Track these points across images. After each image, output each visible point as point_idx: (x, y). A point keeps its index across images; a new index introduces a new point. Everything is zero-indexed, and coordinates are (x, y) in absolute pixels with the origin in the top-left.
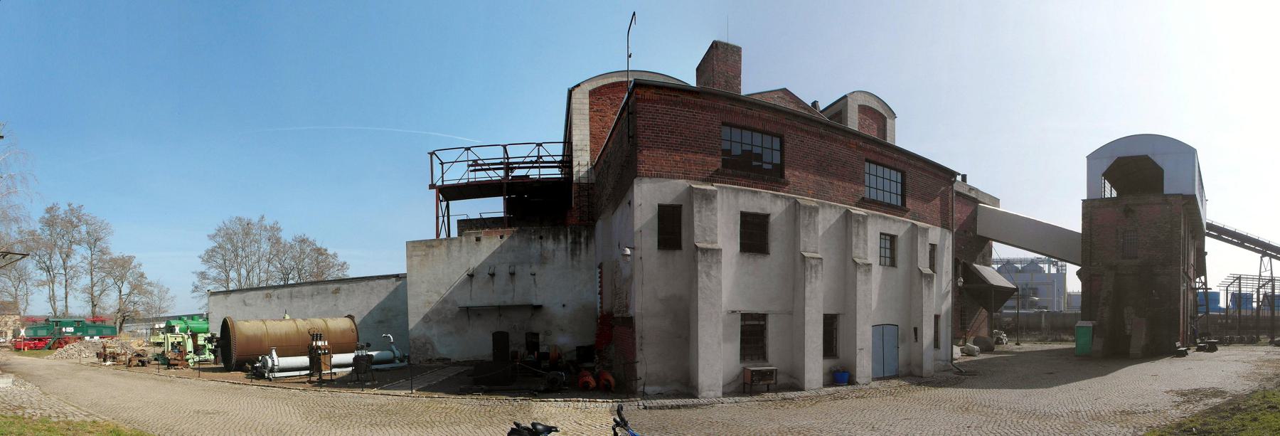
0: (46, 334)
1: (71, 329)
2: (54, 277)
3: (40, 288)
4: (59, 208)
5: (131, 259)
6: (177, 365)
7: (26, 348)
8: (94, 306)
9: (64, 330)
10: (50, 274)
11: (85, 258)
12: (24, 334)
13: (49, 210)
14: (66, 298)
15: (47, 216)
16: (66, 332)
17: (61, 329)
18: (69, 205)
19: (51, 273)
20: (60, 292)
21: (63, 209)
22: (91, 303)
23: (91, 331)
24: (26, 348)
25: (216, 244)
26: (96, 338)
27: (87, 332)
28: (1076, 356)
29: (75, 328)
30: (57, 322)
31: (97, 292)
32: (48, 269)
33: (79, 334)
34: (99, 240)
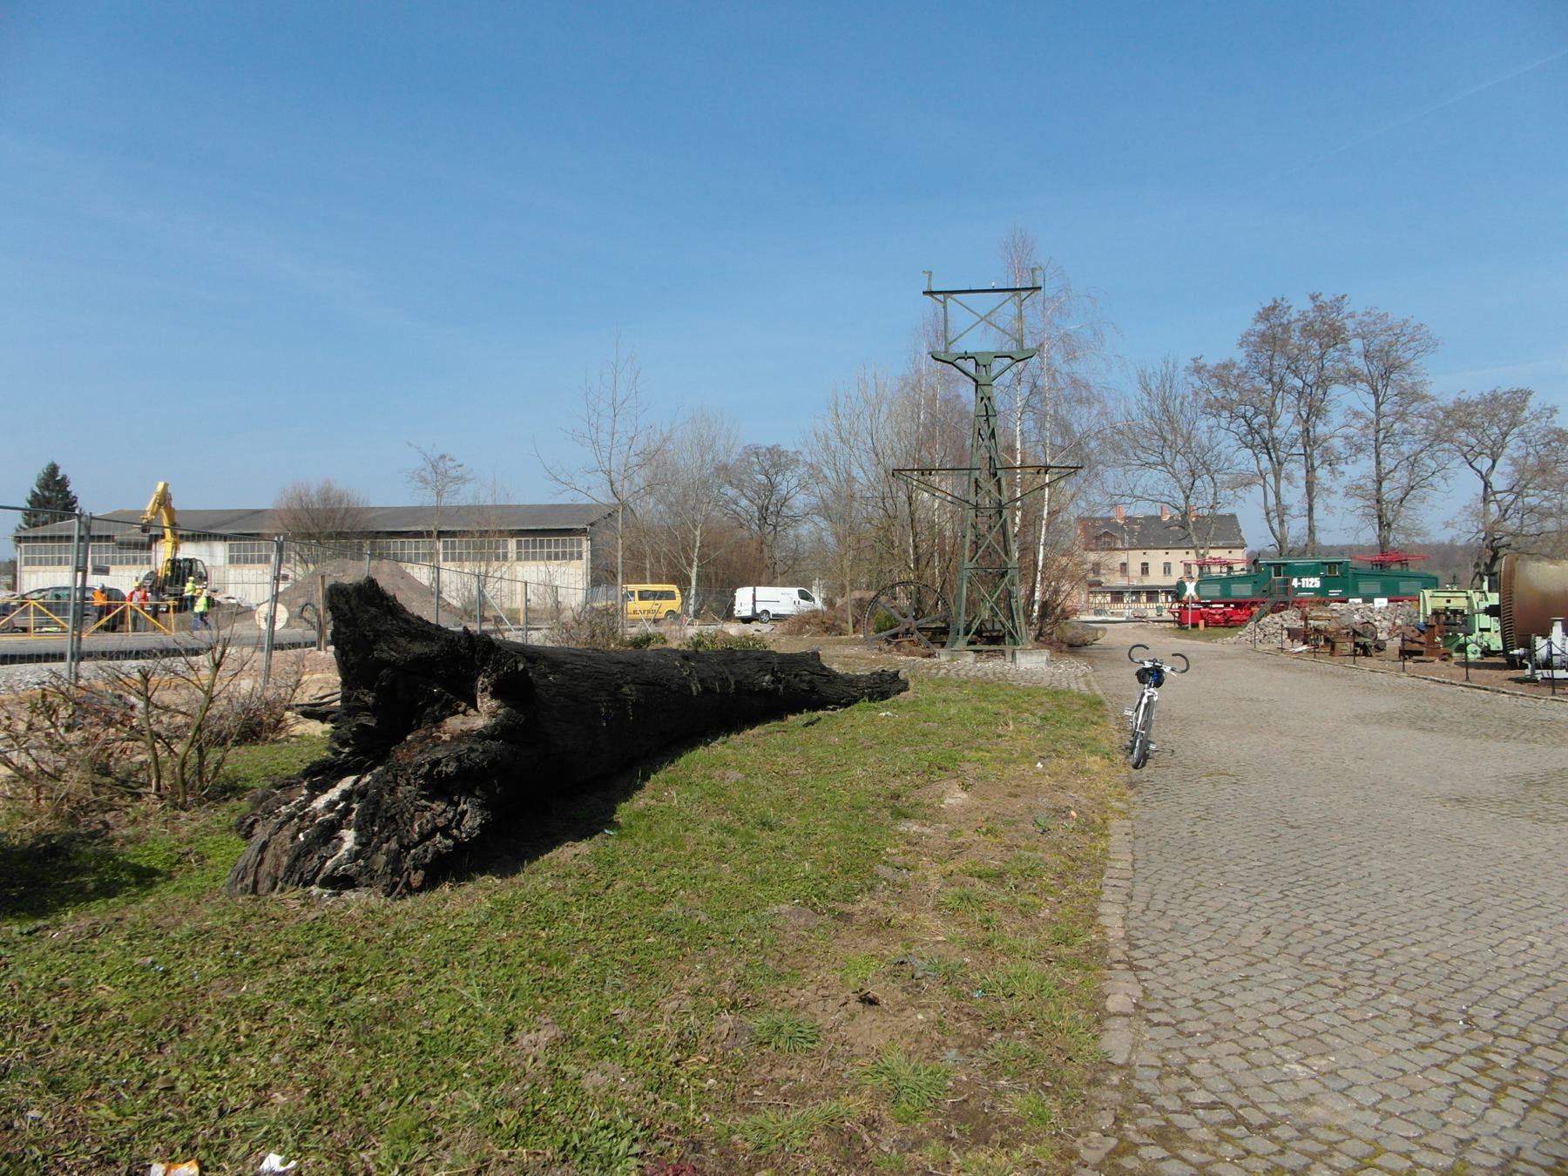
0: (1401, 583)
1: (1315, 582)
2: (1280, 464)
3: (1240, 492)
4: (1289, 307)
5: (1520, 398)
6: (1420, 653)
7: (1202, 623)
8: (1384, 525)
9: (1295, 583)
10: (1271, 458)
11: (1357, 415)
12: (1194, 594)
13: (1267, 314)
14: (1311, 509)
15: (1261, 327)
16: (1300, 589)
17: (1287, 582)
18: (1314, 298)
19: (1273, 455)
20: (1294, 496)
21: (1299, 306)
22: (1376, 520)
23: (1364, 587)
24: (1202, 623)
25: (814, 500)
26: (1381, 602)
27: (1356, 588)
28: (1119, 660)
29: (1323, 579)
30: (1278, 567)
31: (1390, 491)
32: (1269, 446)
33: (1334, 593)
34: (1401, 367)
